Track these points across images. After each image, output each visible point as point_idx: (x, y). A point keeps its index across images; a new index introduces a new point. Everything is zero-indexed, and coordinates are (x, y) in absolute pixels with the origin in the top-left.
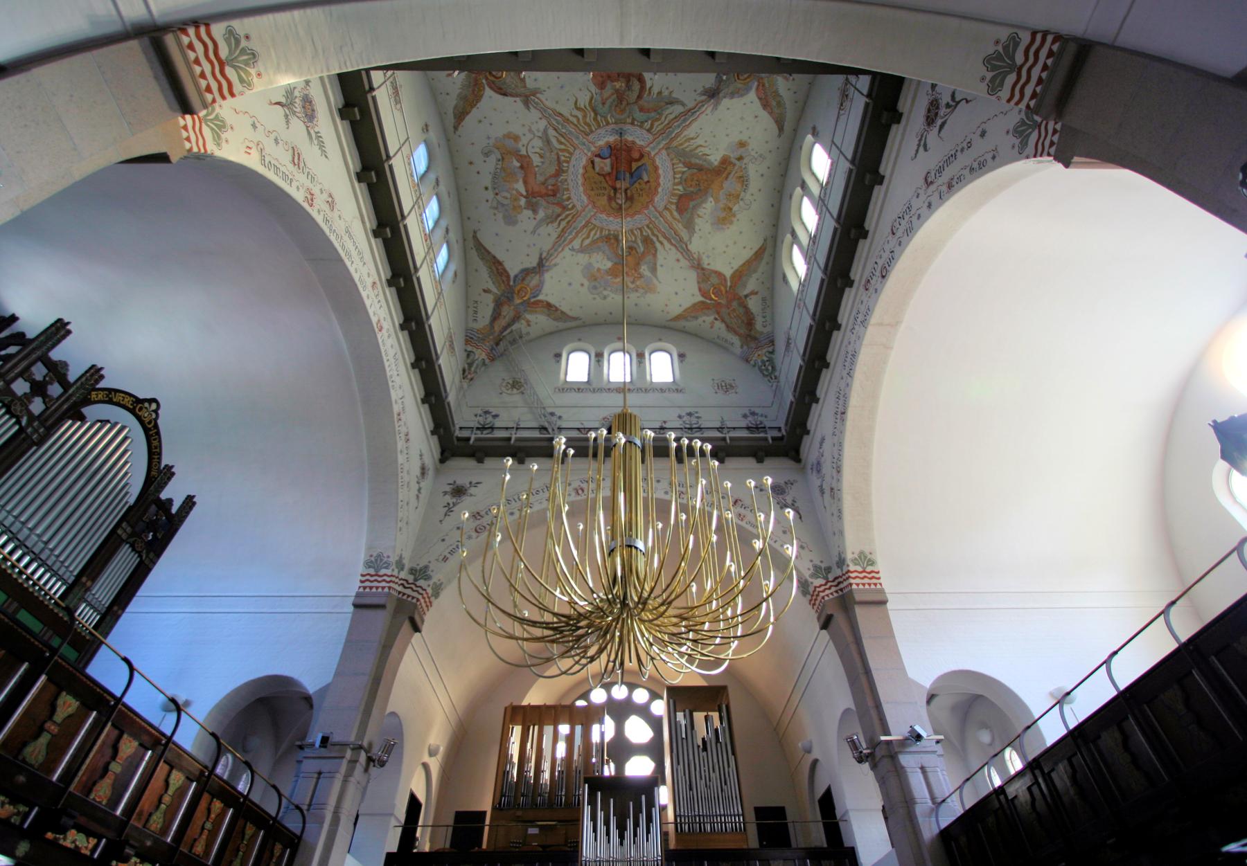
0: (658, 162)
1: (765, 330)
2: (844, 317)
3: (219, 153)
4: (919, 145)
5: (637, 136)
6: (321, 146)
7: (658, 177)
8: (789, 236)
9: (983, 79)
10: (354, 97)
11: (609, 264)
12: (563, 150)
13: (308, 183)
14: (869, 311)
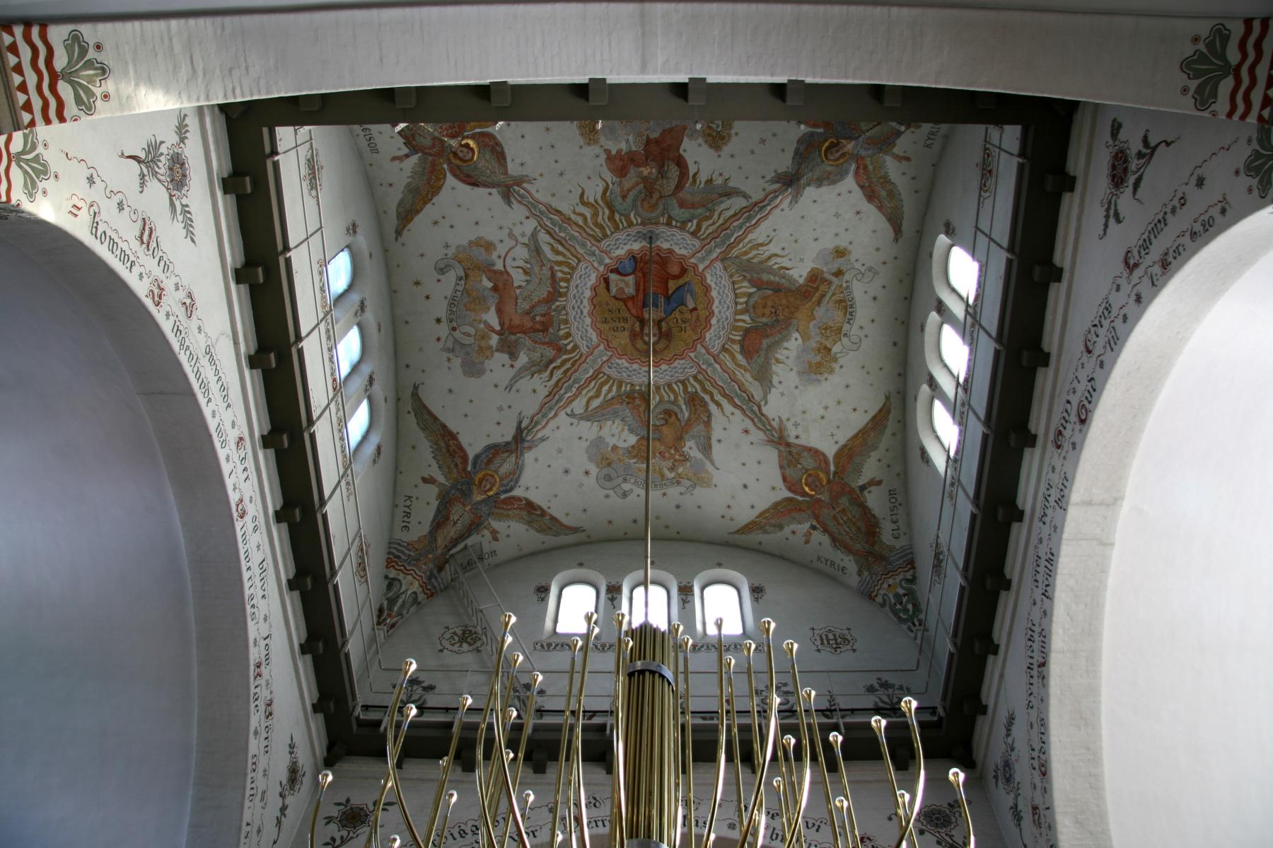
0: (709, 280)
1: (898, 544)
2: (1027, 496)
3: (27, 206)
4: (1107, 217)
5: (676, 243)
6: (188, 225)
7: (711, 302)
8: (925, 388)
9: (1185, 90)
10: (246, 131)
11: (632, 439)
12: (559, 263)
13: (157, 272)
14: (1066, 482)
